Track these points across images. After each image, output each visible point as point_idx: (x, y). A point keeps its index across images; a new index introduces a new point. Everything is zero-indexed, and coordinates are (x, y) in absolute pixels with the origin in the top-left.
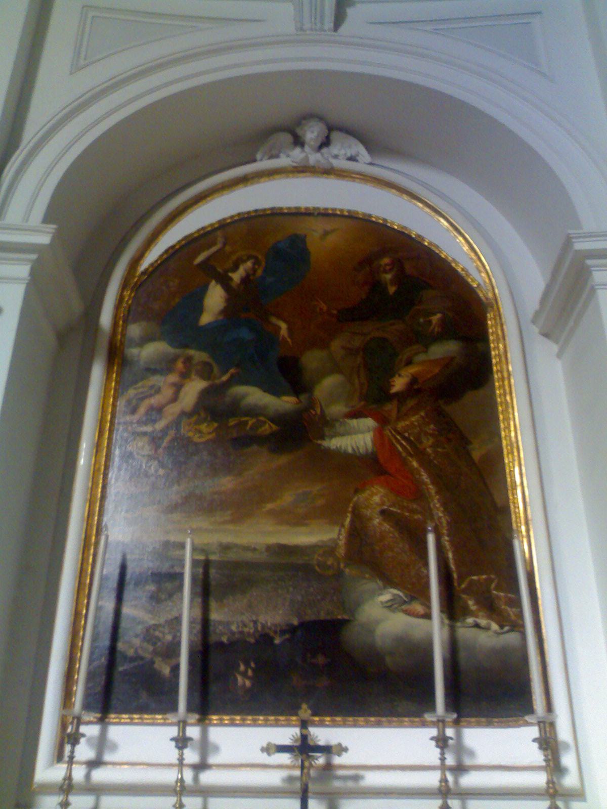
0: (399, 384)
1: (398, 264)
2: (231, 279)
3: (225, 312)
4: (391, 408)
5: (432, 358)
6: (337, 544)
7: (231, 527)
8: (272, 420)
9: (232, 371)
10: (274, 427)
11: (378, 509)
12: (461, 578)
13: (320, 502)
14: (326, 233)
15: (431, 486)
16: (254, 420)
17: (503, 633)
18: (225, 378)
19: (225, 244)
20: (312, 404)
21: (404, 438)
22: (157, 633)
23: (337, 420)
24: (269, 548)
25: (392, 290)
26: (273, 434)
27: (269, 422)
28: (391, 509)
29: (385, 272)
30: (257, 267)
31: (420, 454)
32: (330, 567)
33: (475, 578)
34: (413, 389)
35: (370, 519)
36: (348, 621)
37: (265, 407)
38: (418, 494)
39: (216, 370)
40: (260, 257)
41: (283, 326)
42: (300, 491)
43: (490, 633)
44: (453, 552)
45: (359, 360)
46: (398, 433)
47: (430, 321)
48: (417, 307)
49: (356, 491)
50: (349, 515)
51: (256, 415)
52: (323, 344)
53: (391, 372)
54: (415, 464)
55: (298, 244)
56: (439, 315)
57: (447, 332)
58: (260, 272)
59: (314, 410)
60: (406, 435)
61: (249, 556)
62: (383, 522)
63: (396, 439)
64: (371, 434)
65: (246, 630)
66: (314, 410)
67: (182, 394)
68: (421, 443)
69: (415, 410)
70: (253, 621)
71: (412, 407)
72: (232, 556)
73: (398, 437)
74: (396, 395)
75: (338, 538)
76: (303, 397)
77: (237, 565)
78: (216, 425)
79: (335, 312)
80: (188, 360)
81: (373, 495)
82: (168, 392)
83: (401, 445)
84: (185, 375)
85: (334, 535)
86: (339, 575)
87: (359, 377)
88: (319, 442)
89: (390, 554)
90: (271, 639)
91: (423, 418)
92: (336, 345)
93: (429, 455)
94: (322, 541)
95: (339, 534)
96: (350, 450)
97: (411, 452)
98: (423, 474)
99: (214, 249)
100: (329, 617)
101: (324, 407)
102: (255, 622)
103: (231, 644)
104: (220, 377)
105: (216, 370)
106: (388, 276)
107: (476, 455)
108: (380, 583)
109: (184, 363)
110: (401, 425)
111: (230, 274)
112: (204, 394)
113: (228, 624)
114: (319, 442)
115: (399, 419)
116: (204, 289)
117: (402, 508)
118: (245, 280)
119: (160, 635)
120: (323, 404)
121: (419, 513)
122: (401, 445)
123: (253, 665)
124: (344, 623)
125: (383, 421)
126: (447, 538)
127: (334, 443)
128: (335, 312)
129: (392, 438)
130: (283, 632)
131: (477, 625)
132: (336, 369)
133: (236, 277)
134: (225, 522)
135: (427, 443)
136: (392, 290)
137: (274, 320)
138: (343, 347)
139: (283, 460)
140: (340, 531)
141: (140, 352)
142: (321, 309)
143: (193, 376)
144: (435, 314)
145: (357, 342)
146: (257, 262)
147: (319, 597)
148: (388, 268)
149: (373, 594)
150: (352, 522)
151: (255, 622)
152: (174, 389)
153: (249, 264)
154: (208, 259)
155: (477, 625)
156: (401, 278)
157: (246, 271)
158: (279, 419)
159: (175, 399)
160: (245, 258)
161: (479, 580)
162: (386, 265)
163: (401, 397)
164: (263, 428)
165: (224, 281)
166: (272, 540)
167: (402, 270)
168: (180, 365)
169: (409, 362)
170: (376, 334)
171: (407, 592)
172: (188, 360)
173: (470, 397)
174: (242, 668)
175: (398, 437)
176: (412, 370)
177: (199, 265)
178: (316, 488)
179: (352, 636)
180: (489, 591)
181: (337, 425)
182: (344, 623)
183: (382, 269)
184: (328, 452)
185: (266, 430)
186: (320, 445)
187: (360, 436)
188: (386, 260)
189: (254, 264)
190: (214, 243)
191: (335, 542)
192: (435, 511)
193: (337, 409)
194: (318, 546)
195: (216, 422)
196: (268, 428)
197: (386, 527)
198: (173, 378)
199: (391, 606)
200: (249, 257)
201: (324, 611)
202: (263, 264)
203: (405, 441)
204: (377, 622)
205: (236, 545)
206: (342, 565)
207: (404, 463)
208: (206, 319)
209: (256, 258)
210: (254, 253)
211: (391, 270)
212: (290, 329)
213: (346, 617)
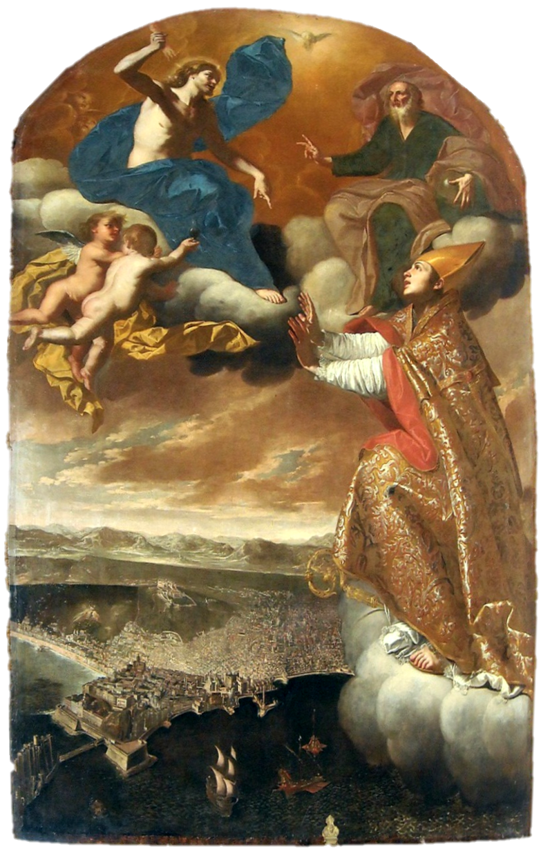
0: (416, 281)
1: (414, 93)
2: (176, 98)
3: (167, 147)
4: (404, 318)
5: (458, 243)
6: (335, 545)
7: (195, 509)
8: (246, 328)
9: (186, 243)
10: (251, 341)
11: (389, 485)
12: (476, 606)
13: (315, 471)
14: (313, 39)
15: (449, 451)
16: (220, 327)
17: (513, 697)
18: (175, 255)
19: (162, 45)
20: (300, 306)
21: (424, 370)
22: (105, 695)
23: (335, 334)
24: (248, 547)
25: (406, 132)
26: (249, 351)
27: (242, 332)
28: (403, 487)
29: (397, 103)
30: (214, 81)
31: (438, 395)
32: (327, 583)
33: (490, 605)
34: (432, 293)
35: (377, 503)
36: (349, 677)
37: (235, 307)
38: (435, 467)
39: (161, 242)
40: (218, 67)
41: (259, 176)
42: (287, 451)
43: (499, 697)
44: (469, 562)
45: (365, 237)
46: (416, 362)
47: (456, 184)
48: (443, 162)
49: (361, 456)
50: (352, 494)
51: (220, 319)
52: (314, 210)
53: (406, 262)
54: (433, 413)
55: (272, 48)
56: (467, 177)
57: (477, 206)
58: (218, 90)
59: (305, 316)
60: (424, 363)
61: (225, 562)
62: (391, 509)
63: (411, 368)
64: (381, 357)
65: (223, 691)
66: (305, 316)
67: (110, 277)
68: (442, 378)
69: (435, 322)
70: (231, 675)
71: (431, 319)
72: (199, 560)
73: (414, 366)
74: (413, 296)
75: (337, 534)
76: (289, 292)
77: (208, 576)
78: (165, 331)
79: (329, 159)
80: (117, 222)
81: (380, 463)
82: (88, 275)
83: (418, 379)
84: (113, 247)
85: (331, 529)
86: (339, 597)
87: (365, 264)
88: (312, 369)
89: (400, 563)
90: (255, 708)
91: (443, 337)
92: (333, 211)
93: (450, 400)
94: (316, 538)
95: (338, 528)
96: (353, 386)
97: (430, 394)
98: (442, 430)
99: (145, 51)
100: (325, 672)
101: (317, 311)
102: (234, 677)
103: (206, 716)
104: (167, 254)
105: (161, 242)
106: (401, 111)
107: (504, 402)
108: (387, 612)
109: (110, 226)
110: (419, 346)
111: (174, 90)
112: (148, 279)
113: (200, 681)
114: (312, 369)
115: (415, 337)
116: (135, 110)
117: (415, 485)
118: (198, 101)
119: (110, 698)
120: (316, 304)
121: (436, 496)
122: (418, 379)
123: (233, 754)
124: (344, 679)
125: (395, 340)
126: (463, 539)
127: (331, 372)
128: (329, 159)
129: (406, 366)
130: (269, 697)
131: (487, 685)
132: (334, 251)
133: (184, 95)
134: (186, 501)
135: (450, 378)
136: (406, 132)
137: (243, 165)
138: (343, 216)
139: (264, 395)
140: (339, 521)
141: (40, 206)
142: (310, 154)
143: (125, 249)
144: (463, 174)
145: (362, 209)
146: (214, 75)
147: (313, 635)
148: (400, 97)
149: (380, 631)
150: (355, 507)
151: (234, 677)
152: (97, 269)
153: (202, 77)
154: (139, 64)
155: (487, 685)
156: (418, 115)
157: (198, 86)
158: (255, 327)
159: (100, 284)
160: (195, 67)
161: (495, 608)
162: (398, 93)
163: (419, 302)
164: (234, 341)
165: (166, 101)
166: (253, 534)
167: (419, 101)
168: (103, 231)
169: (429, 248)
170: (389, 198)
171: (415, 628)
172: (117, 222)
173: (502, 308)
174: (221, 759)
175: (414, 366)
176: (433, 259)
177: (124, 74)
178: (308, 448)
179: (352, 701)
180: (503, 629)
181: (336, 341)
182: (344, 679)
183: (392, 98)
184: (322, 386)
185: (238, 345)
186: (313, 374)
187: (366, 362)
188: (398, 87)
189: (210, 77)
190: (147, 43)
191: (332, 538)
192: (452, 494)
193: (334, 317)
194: (310, 547)
195: (164, 327)
196: (240, 342)
197: (396, 517)
198: (94, 250)
199: (399, 652)
200: (203, 67)
201: (317, 663)
202: (224, 79)
203: (423, 375)
204: (382, 679)
205: (204, 541)
206: (342, 583)
207: (421, 410)
208: (139, 158)
209: (212, 67)
210: (209, 61)
211: (405, 101)
212: (267, 181)
213: (346, 671)
